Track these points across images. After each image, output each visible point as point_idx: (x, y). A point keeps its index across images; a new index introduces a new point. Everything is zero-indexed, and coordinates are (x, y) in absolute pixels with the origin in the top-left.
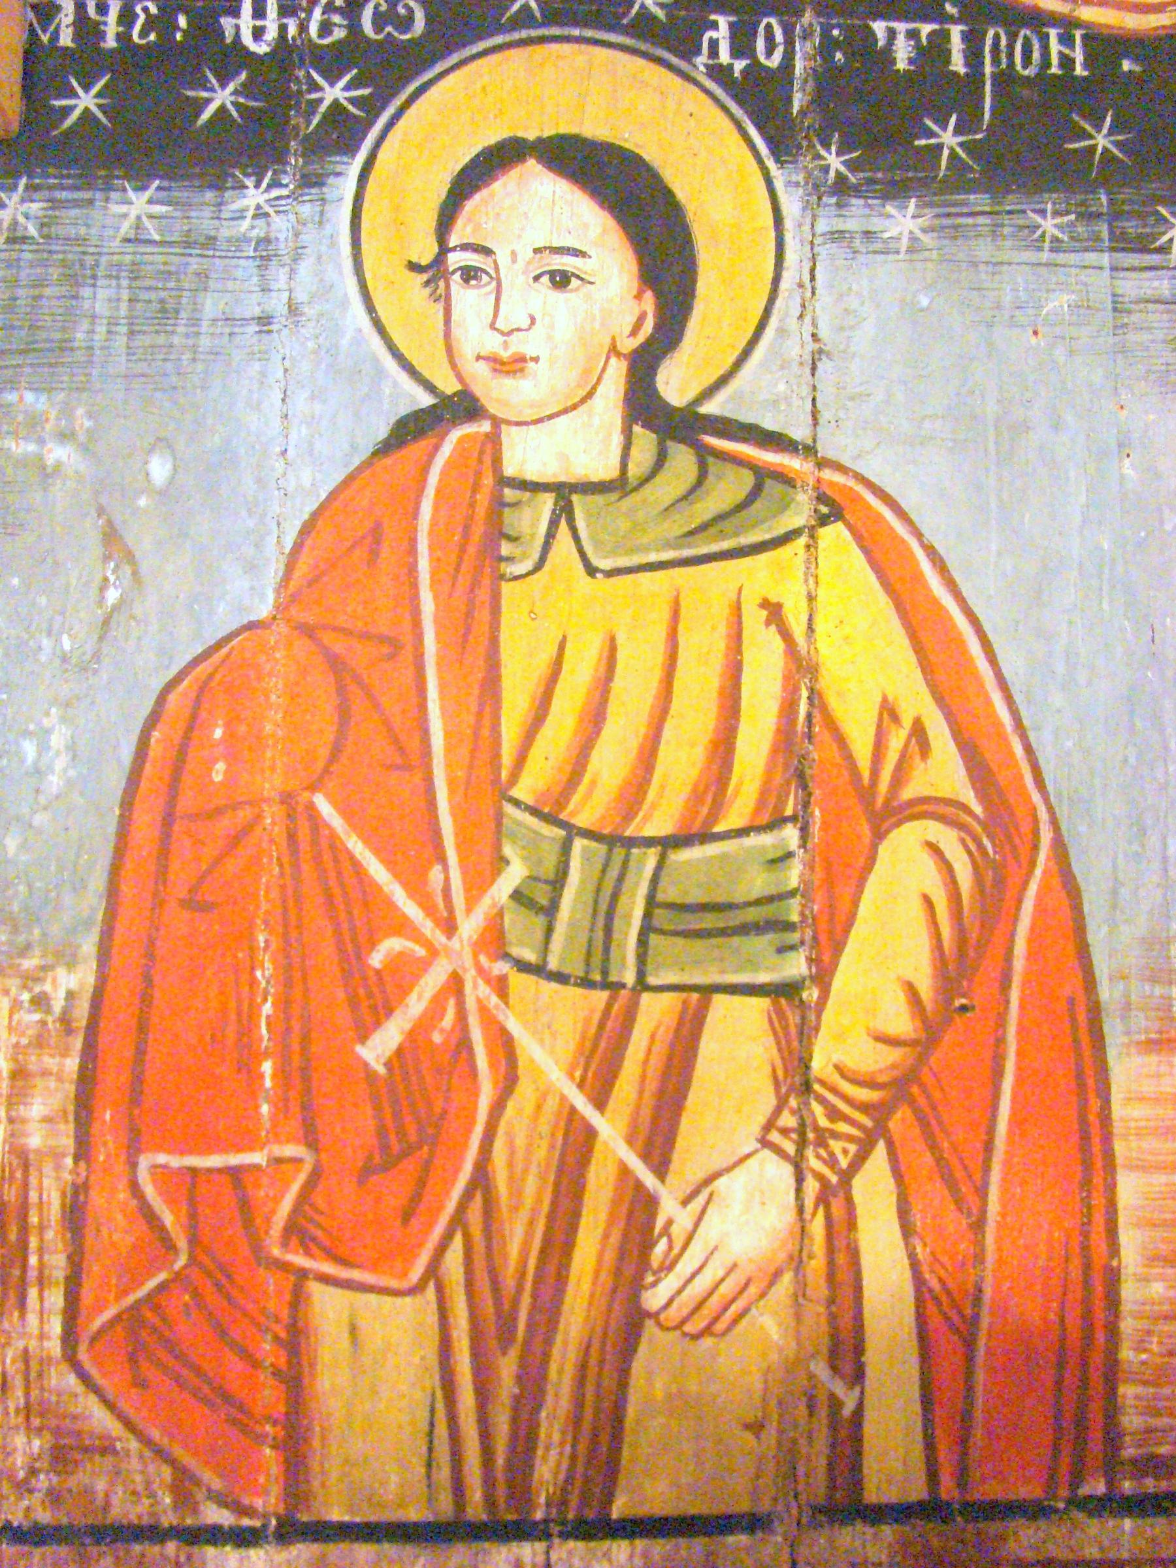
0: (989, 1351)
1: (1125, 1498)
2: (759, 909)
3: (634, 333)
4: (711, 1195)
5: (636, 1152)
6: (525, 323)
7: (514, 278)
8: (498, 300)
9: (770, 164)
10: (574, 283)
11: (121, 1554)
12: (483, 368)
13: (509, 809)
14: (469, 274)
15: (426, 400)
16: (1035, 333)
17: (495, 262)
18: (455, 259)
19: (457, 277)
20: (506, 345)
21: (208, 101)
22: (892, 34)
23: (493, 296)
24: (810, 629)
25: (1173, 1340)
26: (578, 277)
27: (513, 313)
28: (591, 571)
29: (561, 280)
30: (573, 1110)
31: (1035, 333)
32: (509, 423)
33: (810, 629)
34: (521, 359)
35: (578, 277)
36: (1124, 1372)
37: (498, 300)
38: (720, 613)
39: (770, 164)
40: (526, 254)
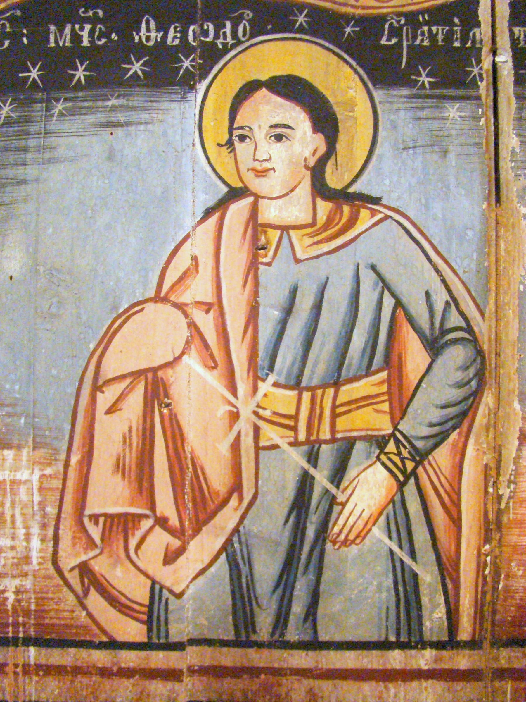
1: (154, 644)
9: (370, 85)
10: (284, 139)
12: (251, 174)
13: (331, 392)
14: (242, 138)
16: (11, 278)
20: (261, 165)
22: (438, 29)
25: (2, 532)
26: (286, 138)
28: (297, 261)
29: (279, 138)
31: (11, 278)
32: (264, 198)
34: (267, 170)
35: (286, 138)
36: (380, 636)
38: (350, 273)
39: (370, 85)
40: (265, 129)
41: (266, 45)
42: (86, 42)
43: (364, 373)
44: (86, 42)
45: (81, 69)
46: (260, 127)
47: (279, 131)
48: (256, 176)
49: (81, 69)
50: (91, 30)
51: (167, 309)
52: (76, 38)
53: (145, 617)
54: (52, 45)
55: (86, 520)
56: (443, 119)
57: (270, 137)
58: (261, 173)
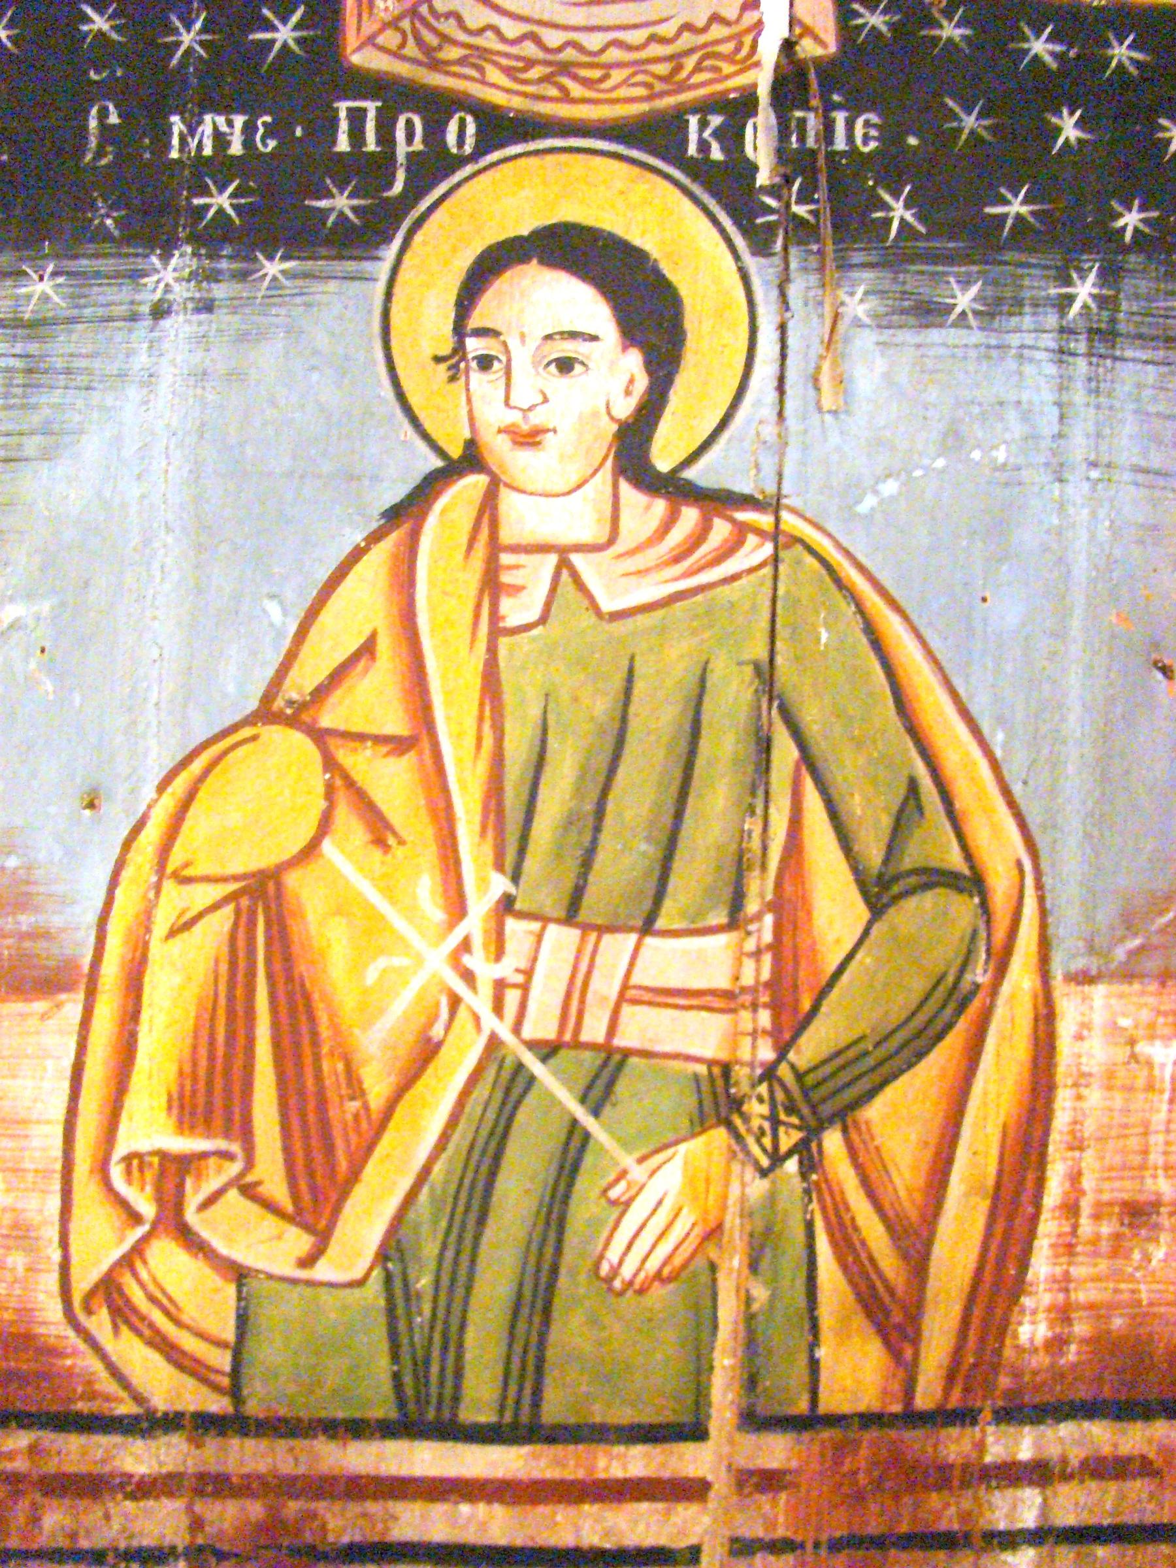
0: (924, 1394)
2: (414, 67)
3: (628, 393)
4: (254, 738)
5: (596, 1141)
6: (540, 399)
7: (522, 357)
8: (508, 386)
10: (578, 368)
11: (930, 1450)
14: (485, 362)
15: (439, 463)
17: (505, 344)
18: (474, 346)
19: (474, 364)
21: (200, 33)
23: (503, 381)
24: (605, 459)
26: (583, 363)
27: (523, 394)
29: (565, 365)
30: (575, 1122)
32: (507, 485)
33: (605, 459)
35: (583, 363)
37: (508, 386)
40: (534, 341)
41: (598, 161)
42: (236, 149)
43: (633, 1060)
44: (236, 149)
45: (1024, 210)
46: (523, 337)
47: (568, 348)
48: (515, 443)
49: (1024, 210)
50: (246, 124)
51: (298, 740)
52: (221, 140)
53: (226, 1381)
54: (174, 154)
55: (116, 1173)
56: (26, 1136)
57: (549, 364)
58: (529, 439)
